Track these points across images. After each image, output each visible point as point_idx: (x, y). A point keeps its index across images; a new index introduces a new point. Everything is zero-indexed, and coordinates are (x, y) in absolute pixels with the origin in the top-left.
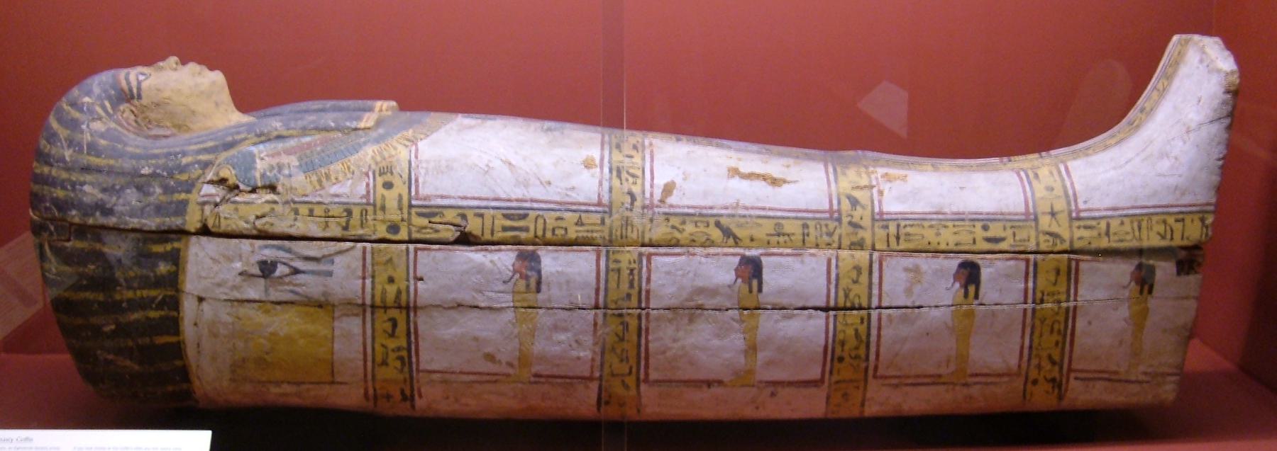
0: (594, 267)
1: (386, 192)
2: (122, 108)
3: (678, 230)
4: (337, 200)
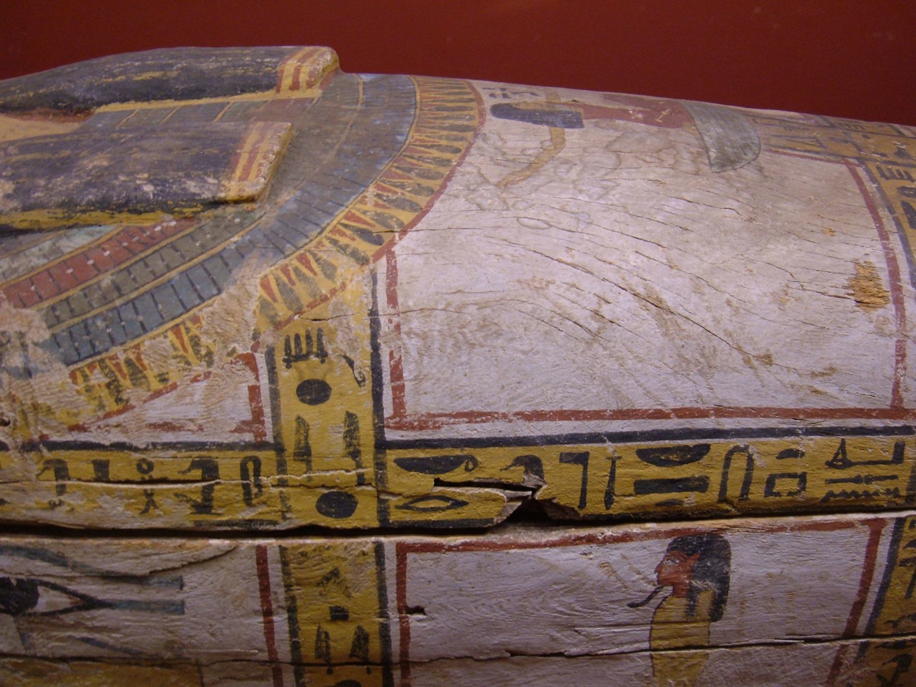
0: (861, 560)
1: (309, 412)
4: (169, 437)
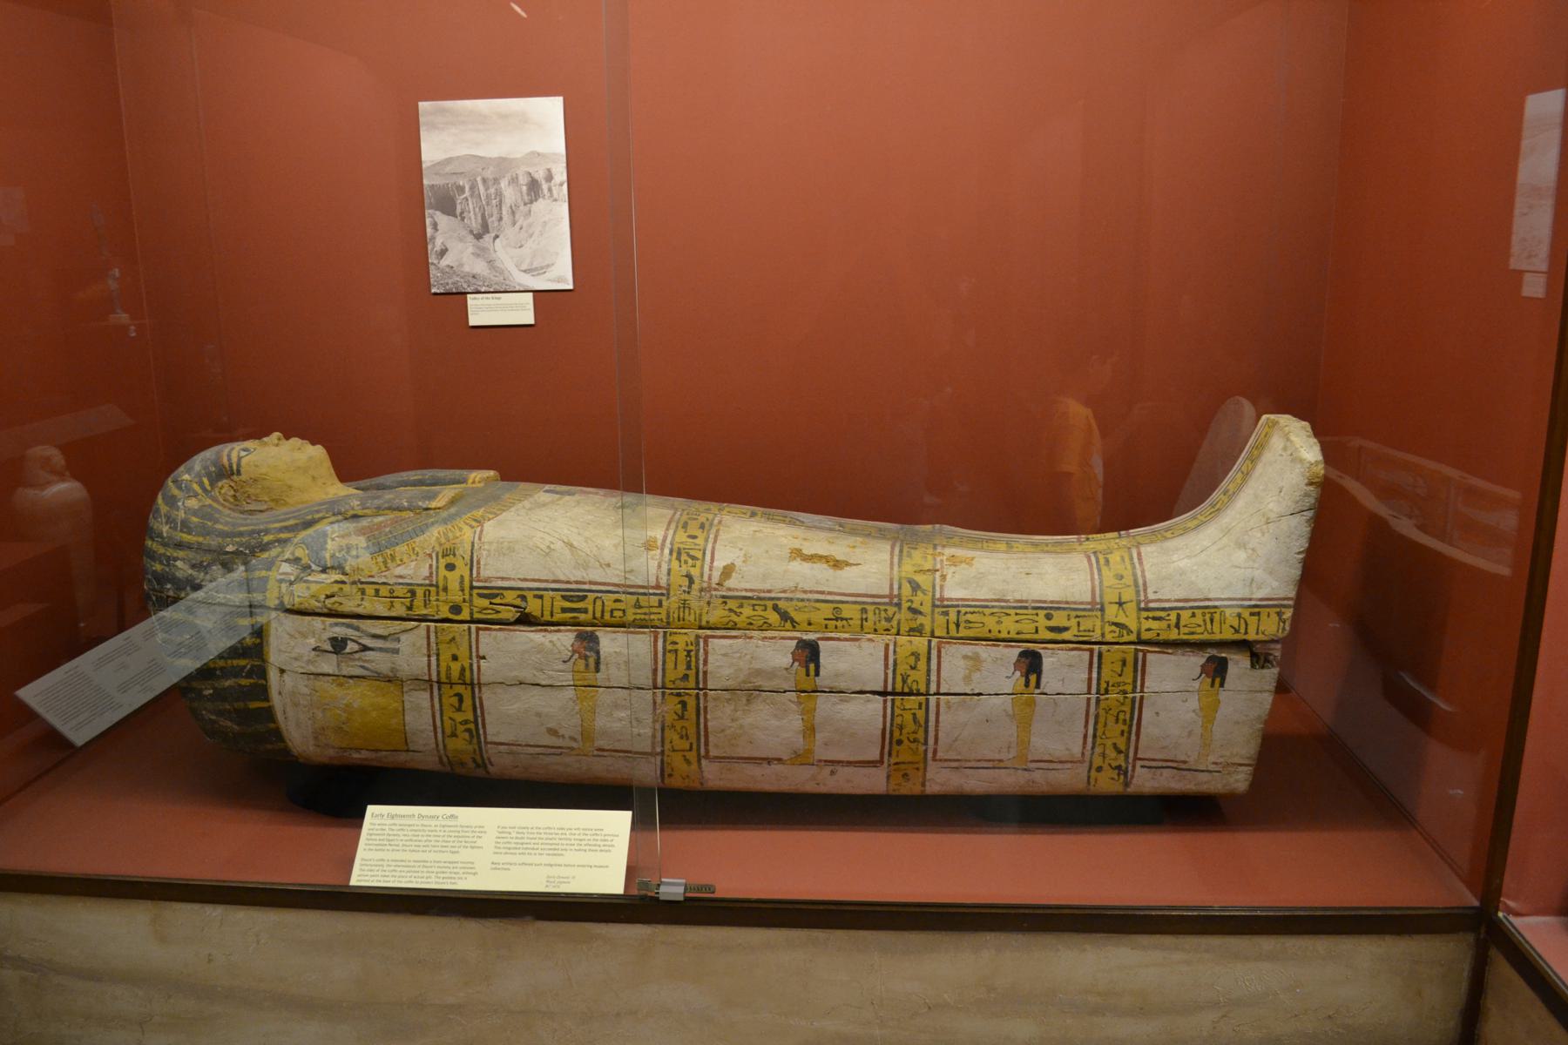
1: (448, 574)
2: (220, 484)
3: (735, 613)
4: (401, 581)
